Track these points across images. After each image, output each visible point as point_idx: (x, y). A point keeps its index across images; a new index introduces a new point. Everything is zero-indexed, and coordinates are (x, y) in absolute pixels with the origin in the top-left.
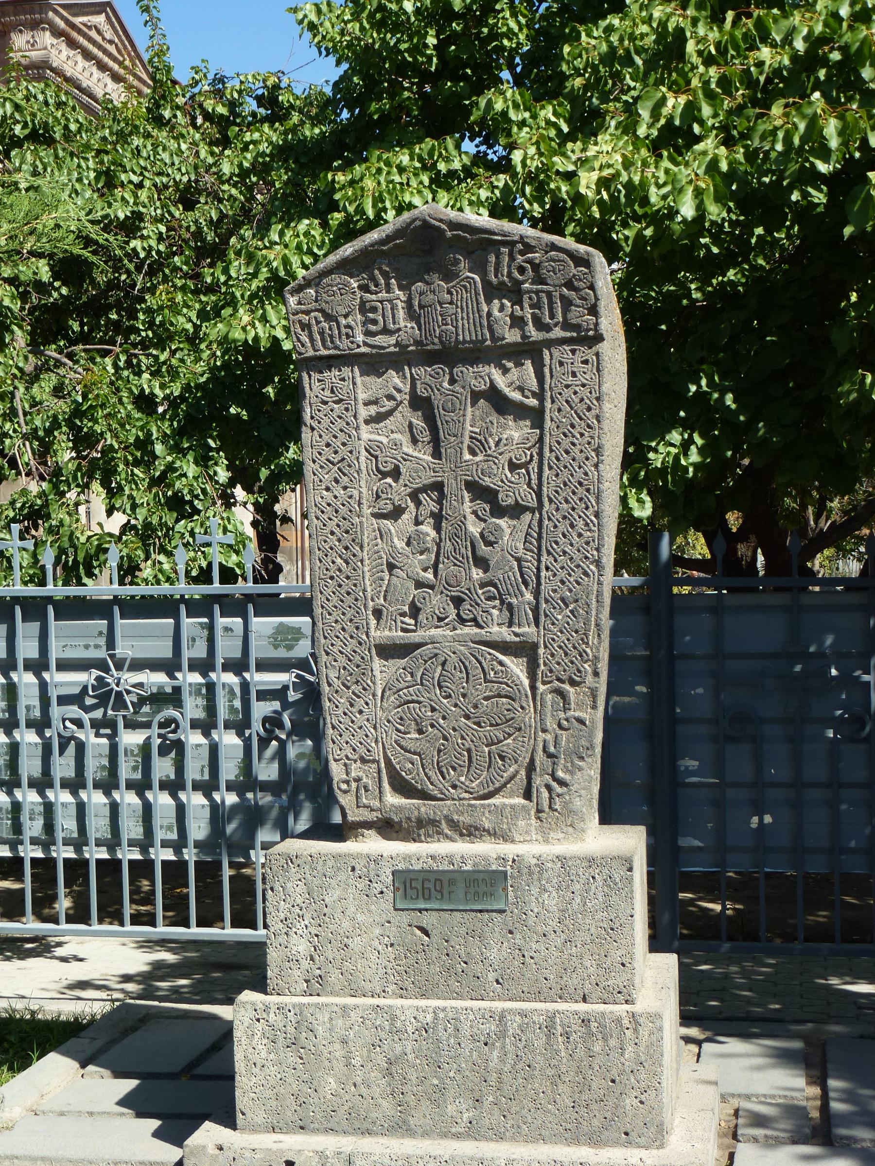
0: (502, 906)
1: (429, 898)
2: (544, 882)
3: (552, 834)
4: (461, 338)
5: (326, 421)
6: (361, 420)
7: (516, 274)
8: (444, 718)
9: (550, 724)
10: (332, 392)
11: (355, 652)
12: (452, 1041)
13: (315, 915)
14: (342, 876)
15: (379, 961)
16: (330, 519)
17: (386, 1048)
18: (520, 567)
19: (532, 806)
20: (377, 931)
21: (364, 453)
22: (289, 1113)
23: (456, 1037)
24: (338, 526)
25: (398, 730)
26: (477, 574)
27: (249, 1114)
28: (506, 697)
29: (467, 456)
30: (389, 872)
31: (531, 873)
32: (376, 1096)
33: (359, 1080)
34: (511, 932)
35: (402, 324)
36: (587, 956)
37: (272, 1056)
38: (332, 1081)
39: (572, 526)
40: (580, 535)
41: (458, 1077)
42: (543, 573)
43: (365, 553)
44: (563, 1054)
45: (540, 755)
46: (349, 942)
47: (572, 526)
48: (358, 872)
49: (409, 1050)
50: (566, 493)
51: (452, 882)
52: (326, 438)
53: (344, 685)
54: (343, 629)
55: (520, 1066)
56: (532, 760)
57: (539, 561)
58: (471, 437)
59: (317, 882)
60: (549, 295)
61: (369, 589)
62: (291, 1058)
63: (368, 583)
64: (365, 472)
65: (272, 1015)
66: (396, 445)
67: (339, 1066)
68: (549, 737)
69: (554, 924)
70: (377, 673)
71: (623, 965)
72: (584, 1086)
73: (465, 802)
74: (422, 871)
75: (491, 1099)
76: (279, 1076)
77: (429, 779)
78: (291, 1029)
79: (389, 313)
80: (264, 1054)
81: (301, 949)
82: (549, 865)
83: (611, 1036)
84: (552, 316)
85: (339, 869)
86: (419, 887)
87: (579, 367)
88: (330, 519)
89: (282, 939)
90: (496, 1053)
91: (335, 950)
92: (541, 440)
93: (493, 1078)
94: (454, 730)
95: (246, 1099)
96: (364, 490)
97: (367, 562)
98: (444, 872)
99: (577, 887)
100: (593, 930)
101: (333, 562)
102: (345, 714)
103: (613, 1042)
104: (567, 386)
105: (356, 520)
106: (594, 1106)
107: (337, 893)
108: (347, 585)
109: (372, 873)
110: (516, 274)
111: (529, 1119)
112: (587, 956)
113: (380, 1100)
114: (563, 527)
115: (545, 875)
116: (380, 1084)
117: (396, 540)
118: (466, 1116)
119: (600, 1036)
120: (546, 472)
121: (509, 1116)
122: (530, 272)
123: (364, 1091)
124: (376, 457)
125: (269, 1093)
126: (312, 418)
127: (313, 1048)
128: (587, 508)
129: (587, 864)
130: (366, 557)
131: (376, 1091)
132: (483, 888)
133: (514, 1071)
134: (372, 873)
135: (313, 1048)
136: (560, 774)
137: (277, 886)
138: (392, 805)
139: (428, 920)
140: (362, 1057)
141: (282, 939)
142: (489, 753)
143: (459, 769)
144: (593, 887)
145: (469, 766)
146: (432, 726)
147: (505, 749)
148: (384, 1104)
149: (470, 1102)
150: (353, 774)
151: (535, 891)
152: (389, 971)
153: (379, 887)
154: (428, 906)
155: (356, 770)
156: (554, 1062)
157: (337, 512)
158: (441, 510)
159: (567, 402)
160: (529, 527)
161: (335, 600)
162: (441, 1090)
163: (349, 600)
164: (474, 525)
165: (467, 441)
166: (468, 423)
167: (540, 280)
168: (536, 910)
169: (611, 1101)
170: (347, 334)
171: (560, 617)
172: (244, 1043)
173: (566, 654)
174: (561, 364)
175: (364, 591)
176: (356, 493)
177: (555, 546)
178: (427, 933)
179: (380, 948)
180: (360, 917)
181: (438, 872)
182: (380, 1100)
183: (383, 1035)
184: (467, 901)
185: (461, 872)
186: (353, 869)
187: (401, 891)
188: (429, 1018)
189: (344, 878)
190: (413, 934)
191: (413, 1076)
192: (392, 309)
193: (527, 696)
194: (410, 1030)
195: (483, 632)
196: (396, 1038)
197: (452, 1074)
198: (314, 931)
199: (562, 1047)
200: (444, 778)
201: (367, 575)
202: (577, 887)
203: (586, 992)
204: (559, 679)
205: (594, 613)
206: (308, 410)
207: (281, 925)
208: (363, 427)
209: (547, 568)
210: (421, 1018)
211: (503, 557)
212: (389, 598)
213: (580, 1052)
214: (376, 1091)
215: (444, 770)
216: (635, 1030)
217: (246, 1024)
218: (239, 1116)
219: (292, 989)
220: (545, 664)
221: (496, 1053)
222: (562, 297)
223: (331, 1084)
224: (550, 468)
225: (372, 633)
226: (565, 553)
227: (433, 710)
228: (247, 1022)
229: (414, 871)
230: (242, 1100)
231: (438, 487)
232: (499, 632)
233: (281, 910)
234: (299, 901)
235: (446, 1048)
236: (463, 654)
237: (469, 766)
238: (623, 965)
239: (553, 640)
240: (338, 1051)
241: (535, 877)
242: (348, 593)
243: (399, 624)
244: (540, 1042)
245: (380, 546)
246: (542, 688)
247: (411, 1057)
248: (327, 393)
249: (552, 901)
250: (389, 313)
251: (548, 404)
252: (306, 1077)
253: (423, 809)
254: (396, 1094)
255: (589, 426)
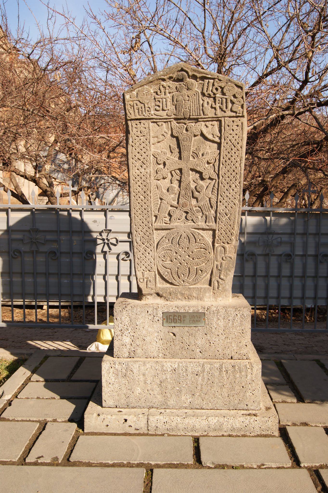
0: (203, 325)
1: (176, 322)
2: (218, 317)
3: (218, 298)
4: (191, 114)
5: (138, 144)
6: (151, 144)
7: (215, 91)
8: (180, 256)
9: (220, 259)
10: (141, 133)
11: (147, 231)
12: (184, 374)
13: (133, 329)
14: (143, 314)
15: (157, 345)
16: (138, 181)
17: (160, 377)
18: (210, 201)
19: (212, 288)
20: (156, 334)
21: (152, 156)
22: (122, 401)
23: (186, 372)
24: (142, 184)
25: (163, 260)
26: (194, 202)
27: (107, 401)
28: (204, 249)
29: (191, 158)
30: (161, 313)
31: (214, 313)
32: (156, 394)
33: (149, 388)
34: (206, 334)
35: (169, 108)
36: (233, 343)
37: (116, 380)
38: (139, 389)
39: (230, 186)
40: (233, 190)
41: (186, 387)
42: (219, 203)
43: (152, 194)
44: (225, 378)
45: (215, 270)
46: (145, 338)
47: (230, 186)
48: (149, 313)
49: (168, 377)
50: (228, 174)
51: (184, 317)
52: (138, 150)
53: (143, 243)
54: (143, 222)
55: (209, 383)
56: (212, 272)
57: (217, 199)
58: (193, 152)
59: (134, 316)
60: (226, 99)
61: (153, 208)
62: (124, 381)
63: (152, 205)
64: (152, 163)
65: (117, 365)
66: (165, 153)
67: (142, 384)
68: (219, 264)
69: (222, 331)
70: (155, 239)
71: (246, 346)
72: (233, 389)
73: (187, 287)
74: (174, 312)
75: (198, 394)
76: (119, 388)
77: (174, 278)
78: (124, 371)
79: (165, 103)
80: (113, 380)
81: (127, 341)
82: (221, 310)
83: (243, 371)
84: (226, 108)
85: (142, 312)
86: (172, 318)
87: (235, 128)
88: (138, 181)
89: (120, 337)
90: (200, 378)
91: (140, 341)
92: (220, 154)
93: (199, 388)
94: (184, 260)
95: (106, 396)
96: (152, 170)
97: (152, 197)
98: (181, 313)
99: (230, 318)
100: (236, 334)
101: (139, 197)
102: (143, 254)
103: (243, 373)
104: (230, 134)
105: (148, 181)
106: (236, 396)
107: (141, 321)
108: (145, 206)
109: (155, 314)
110: (215, 91)
111: (212, 401)
112: (233, 343)
113: (157, 396)
114: (227, 187)
115: (219, 314)
116: (157, 390)
117: (163, 189)
118: (189, 400)
119: (239, 372)
120: (221, 165)
121: (204, 400)
122: (220, 90)
123: (151, 392)
124: (157, 158)
125: (115, 394)
126: (132, 142)
127: (132, 377)
128: (236, 180)
129: (234, 310)
130: (152, 196)
131: (156, 392)
132: (196, 319)
133: (207, 384)
134: (155, 314)
135: (132, 377)
136: (222, 277)
137: (118, 318)
138: (160, 288)
139: (175, 330)
140: (151, 380)
141: (120, 337)
142: (196, 269)
143: (185, 275)
144: (236, 318)
145: (189, 274)
146: (176, 259)
147: (202, 268)
148: (159, 397)
149: (191, 395)
150: (145, 276)
151: (215, 319)
152: (160, 349)
153: (157, 318)
154: (175, 325)
155: (147, 274)
156: (221, 381)
157: (141, 178)
158: (181, 179)
159: (230, 140)
160: (214, 186)
161: (140, 211)
162: (180, 391)
163: (145, 212)
164: (193, 184)
165: (191, 153)
166: (192, 146)
167: (223, 94)
168: (215, 326)
169: (242, 394)
170: (148, 111)
171: (224, 220)
172: (106, 376)
173: (226, 234)
174: (228, 126)
175: (151, 208)
176: (149, 172)
177: (223, 193)
178: (174, 335)
179: (157, 340)
180: (150, 329)
181: (179, 313)
182: (157, 396)
183: (159, 372)
184: (190, 323)
185: (188, 313)
186: (148, 312)
187: (166, 320)
188: (176, 366)
189: (144, 315)
190: (169, 335)
191: (169, 387)
192: (166, 102)
193: (211, 248)
194: (169, 370)
195: (195, 225)
196: (164, 373)
197: (184, 386)
198: (132, 334)
199: (225, 375)
200: (179, 278)
201: (152, 202)
202: (230, 318)
203: (232, 355)
204: (223, 243)
205: (237, 219)
206: (131, 139)
207: (119, 332)
208: (152, 146)
209: (220, 202)
210: (173, 366)
211: (204, 197)
212: (160, 211)
213: (231, 377)
214: (156, 392)
215: (180, 275)
216: (252, 369)
217: (107, 369)
218: (103, 402)
219: (123, 356)
220: (218, 237)
221: (200, 378)
222: (231, 101)
223: (138, 390)
224: (223, 164)
225: (153, 224)
226: (227, 196)
227: (176, 253)
228: (107, 368)
229: (170, 312)
230: (105, 395)
231: (180, 170)
232: (201, 224)
233: (120, 327)
234: (126, 323)
235: (182, 376)
236: (188, 233)
237: (189, 274)
238: (246, 346)
239: (222, 228)
240: (142, 378)
241: (216, 315)
242: (145, 209)
243: (164, 221)
244: (217, 374)
245: (157, 192)
246: (216, 245)
247: (169, 380)
248: (139, 133)
249: (221, 323)
250: (165, 103)
251: (223, 140)
252: (130, 388)
253: (171, 289)
254: (163, 393)
255: (238, 150)
